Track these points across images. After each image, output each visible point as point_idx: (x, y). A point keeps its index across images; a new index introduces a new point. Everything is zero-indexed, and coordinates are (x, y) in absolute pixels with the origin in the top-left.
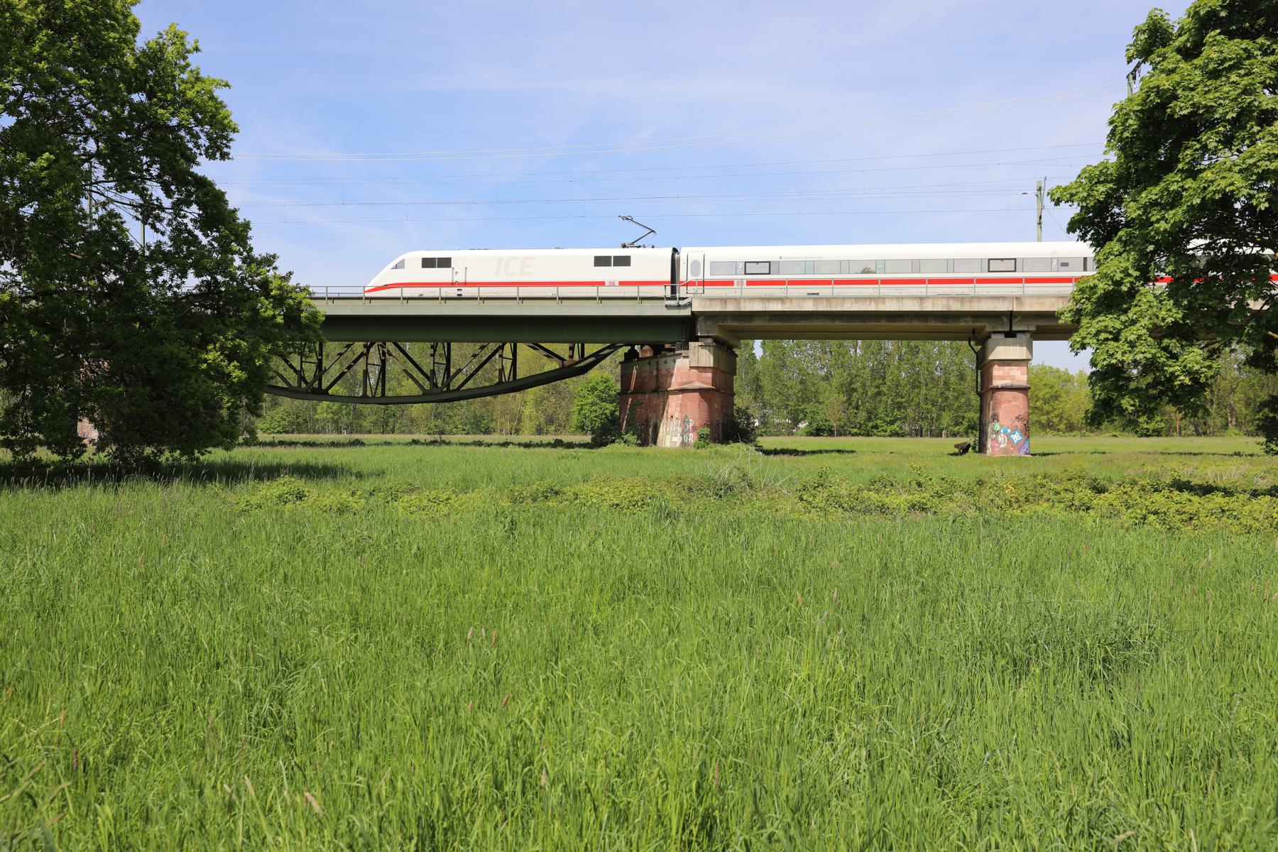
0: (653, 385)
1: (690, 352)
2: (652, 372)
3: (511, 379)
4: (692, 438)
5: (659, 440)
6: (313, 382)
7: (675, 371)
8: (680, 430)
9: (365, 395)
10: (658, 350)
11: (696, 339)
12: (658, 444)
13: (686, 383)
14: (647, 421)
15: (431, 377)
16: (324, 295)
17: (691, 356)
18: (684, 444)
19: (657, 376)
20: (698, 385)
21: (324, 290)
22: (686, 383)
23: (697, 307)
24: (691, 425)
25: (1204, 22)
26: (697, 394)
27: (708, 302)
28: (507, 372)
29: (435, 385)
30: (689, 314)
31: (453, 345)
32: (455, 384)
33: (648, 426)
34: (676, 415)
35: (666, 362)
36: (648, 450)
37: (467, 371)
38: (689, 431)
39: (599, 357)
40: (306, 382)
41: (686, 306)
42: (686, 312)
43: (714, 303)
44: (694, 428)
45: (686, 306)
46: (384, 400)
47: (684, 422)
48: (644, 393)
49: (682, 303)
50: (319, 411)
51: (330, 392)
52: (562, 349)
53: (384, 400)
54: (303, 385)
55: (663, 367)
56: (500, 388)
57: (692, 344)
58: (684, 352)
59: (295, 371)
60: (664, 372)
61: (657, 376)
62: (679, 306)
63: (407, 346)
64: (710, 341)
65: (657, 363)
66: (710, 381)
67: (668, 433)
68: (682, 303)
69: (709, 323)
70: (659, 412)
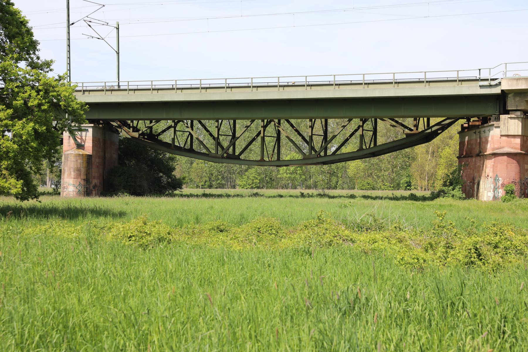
0: (477, 151)
1: (501, 123)
2: (476, 140)
3: (372, 145)
4: (501, 193)
5: (480, 194)
6: (228, 148)
7: (490, 139)
8: (492, 186)
9: (262, 160)
10: (485, 120)
11: (507, 112)
12: (480, 198)
13: (498, 149)
14: (474, 179)
15: (309, 142)
16: (150, 87)
17: (502, 126)
18: (495, 198)
19: (480, 143)
20: (507, 150)
21: (198, 82)
22: (498, 149)
23: (505, 86)
24: (500, 182)
25: (2, 23)
26: (505, 157)
27: (515, 82)
28: (367, 139)
29: (312, 148)
30: (499, 92)
31: (330, 121)
32: (332, 149)
33: (474, 184)
34: (491, 174)
35: (484, 132)
36: (471, 202)
37: (340, 139)
38: (498, 188)
39: (444, 128)
40: (316, 151)
41: (496, 85)
42: (497, 91)
43: (520, 82)
44: (503, 185)
45: (496, 85)
46: (278, 163)
47: (496, 180)
48: (472, 157)
49: (493, 83)
50: (281, 172)
51: (242, 157)
52: (409, 122)
53: (278, 163)
54: (313, 153)
55: (483, 135)
56: (361, 153)
57: (502, 117)
58: (495, 123)
59: (214, 138)
60: (483, 140)
61: (480, 143)
62: (490, 86)
63: (293, 121)
64: (519, 113)
65: (480, 132)
66: (519, 146)
67: (485, 189)
68: (493, 83)
69: (518, 99)
70: (479, 170)
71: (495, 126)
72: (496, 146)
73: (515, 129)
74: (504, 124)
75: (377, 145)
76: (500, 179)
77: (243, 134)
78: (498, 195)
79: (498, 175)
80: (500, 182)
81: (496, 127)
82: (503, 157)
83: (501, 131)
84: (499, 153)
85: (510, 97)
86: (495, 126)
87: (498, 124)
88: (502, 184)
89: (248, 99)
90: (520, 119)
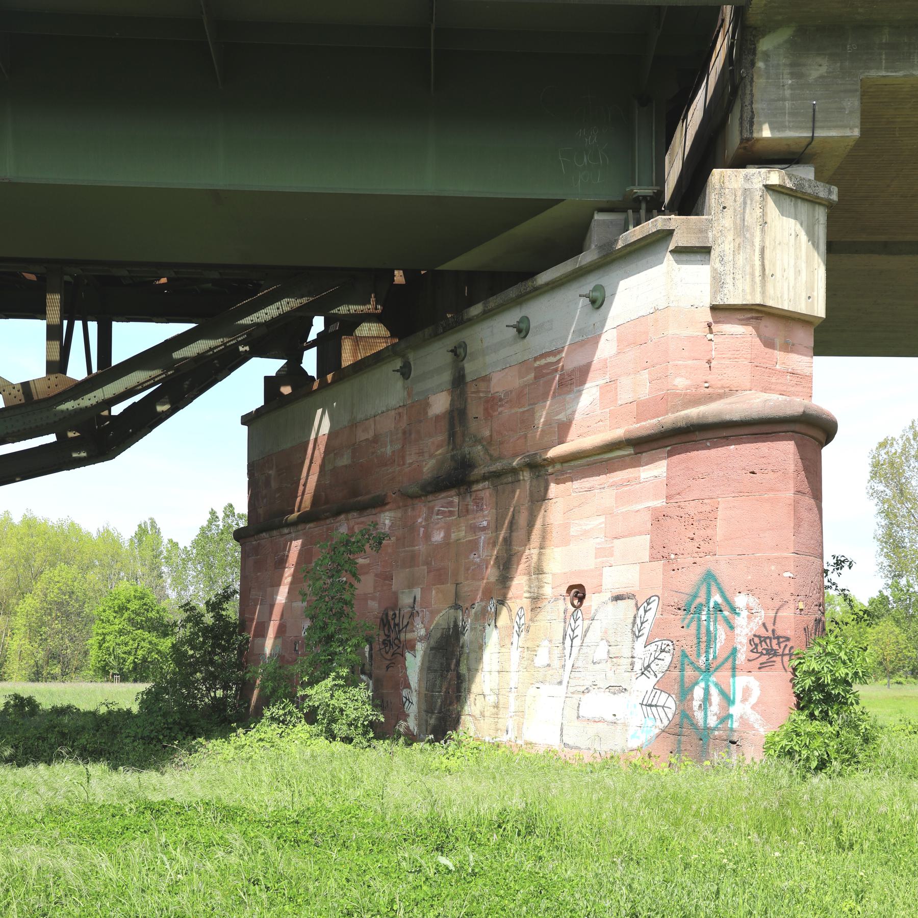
22: (697, 401)
71: (678, 240)
72: (681, 383)
73: (798, 272)
74: (742, 229)
75: (343, 366)
76: (740, 601)
77: (770, 431)
78: (725, 718)
79: (723, 572)
80: (741, 621)
81: (680, 251)
82: (764, 448)
83: (718, 282)
84: (736, 417)
85: (766, 56)
86: (678, 240)
87: (703, 231)
88: (757, 641)
89: (82, 468)
90: (821, 215)
